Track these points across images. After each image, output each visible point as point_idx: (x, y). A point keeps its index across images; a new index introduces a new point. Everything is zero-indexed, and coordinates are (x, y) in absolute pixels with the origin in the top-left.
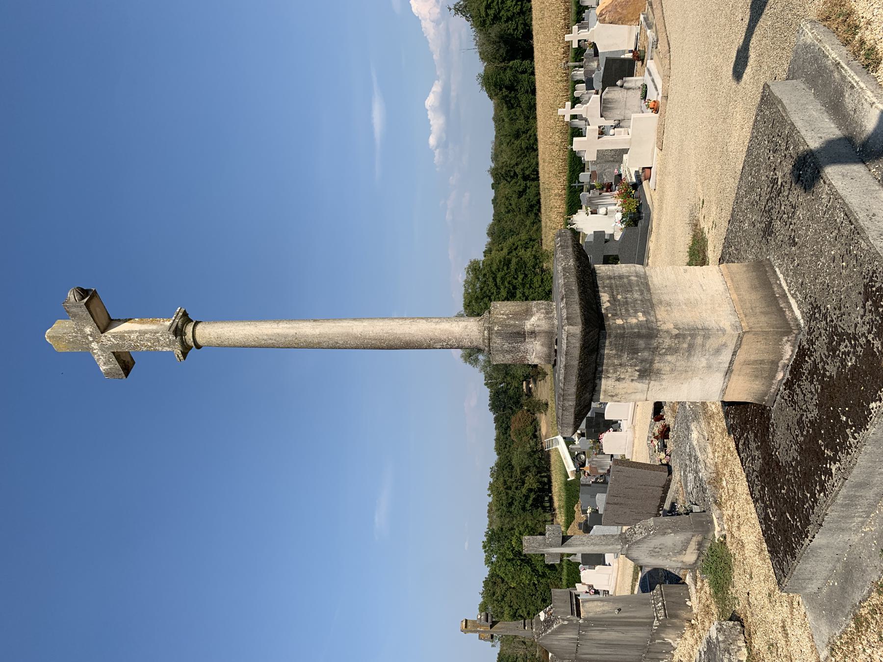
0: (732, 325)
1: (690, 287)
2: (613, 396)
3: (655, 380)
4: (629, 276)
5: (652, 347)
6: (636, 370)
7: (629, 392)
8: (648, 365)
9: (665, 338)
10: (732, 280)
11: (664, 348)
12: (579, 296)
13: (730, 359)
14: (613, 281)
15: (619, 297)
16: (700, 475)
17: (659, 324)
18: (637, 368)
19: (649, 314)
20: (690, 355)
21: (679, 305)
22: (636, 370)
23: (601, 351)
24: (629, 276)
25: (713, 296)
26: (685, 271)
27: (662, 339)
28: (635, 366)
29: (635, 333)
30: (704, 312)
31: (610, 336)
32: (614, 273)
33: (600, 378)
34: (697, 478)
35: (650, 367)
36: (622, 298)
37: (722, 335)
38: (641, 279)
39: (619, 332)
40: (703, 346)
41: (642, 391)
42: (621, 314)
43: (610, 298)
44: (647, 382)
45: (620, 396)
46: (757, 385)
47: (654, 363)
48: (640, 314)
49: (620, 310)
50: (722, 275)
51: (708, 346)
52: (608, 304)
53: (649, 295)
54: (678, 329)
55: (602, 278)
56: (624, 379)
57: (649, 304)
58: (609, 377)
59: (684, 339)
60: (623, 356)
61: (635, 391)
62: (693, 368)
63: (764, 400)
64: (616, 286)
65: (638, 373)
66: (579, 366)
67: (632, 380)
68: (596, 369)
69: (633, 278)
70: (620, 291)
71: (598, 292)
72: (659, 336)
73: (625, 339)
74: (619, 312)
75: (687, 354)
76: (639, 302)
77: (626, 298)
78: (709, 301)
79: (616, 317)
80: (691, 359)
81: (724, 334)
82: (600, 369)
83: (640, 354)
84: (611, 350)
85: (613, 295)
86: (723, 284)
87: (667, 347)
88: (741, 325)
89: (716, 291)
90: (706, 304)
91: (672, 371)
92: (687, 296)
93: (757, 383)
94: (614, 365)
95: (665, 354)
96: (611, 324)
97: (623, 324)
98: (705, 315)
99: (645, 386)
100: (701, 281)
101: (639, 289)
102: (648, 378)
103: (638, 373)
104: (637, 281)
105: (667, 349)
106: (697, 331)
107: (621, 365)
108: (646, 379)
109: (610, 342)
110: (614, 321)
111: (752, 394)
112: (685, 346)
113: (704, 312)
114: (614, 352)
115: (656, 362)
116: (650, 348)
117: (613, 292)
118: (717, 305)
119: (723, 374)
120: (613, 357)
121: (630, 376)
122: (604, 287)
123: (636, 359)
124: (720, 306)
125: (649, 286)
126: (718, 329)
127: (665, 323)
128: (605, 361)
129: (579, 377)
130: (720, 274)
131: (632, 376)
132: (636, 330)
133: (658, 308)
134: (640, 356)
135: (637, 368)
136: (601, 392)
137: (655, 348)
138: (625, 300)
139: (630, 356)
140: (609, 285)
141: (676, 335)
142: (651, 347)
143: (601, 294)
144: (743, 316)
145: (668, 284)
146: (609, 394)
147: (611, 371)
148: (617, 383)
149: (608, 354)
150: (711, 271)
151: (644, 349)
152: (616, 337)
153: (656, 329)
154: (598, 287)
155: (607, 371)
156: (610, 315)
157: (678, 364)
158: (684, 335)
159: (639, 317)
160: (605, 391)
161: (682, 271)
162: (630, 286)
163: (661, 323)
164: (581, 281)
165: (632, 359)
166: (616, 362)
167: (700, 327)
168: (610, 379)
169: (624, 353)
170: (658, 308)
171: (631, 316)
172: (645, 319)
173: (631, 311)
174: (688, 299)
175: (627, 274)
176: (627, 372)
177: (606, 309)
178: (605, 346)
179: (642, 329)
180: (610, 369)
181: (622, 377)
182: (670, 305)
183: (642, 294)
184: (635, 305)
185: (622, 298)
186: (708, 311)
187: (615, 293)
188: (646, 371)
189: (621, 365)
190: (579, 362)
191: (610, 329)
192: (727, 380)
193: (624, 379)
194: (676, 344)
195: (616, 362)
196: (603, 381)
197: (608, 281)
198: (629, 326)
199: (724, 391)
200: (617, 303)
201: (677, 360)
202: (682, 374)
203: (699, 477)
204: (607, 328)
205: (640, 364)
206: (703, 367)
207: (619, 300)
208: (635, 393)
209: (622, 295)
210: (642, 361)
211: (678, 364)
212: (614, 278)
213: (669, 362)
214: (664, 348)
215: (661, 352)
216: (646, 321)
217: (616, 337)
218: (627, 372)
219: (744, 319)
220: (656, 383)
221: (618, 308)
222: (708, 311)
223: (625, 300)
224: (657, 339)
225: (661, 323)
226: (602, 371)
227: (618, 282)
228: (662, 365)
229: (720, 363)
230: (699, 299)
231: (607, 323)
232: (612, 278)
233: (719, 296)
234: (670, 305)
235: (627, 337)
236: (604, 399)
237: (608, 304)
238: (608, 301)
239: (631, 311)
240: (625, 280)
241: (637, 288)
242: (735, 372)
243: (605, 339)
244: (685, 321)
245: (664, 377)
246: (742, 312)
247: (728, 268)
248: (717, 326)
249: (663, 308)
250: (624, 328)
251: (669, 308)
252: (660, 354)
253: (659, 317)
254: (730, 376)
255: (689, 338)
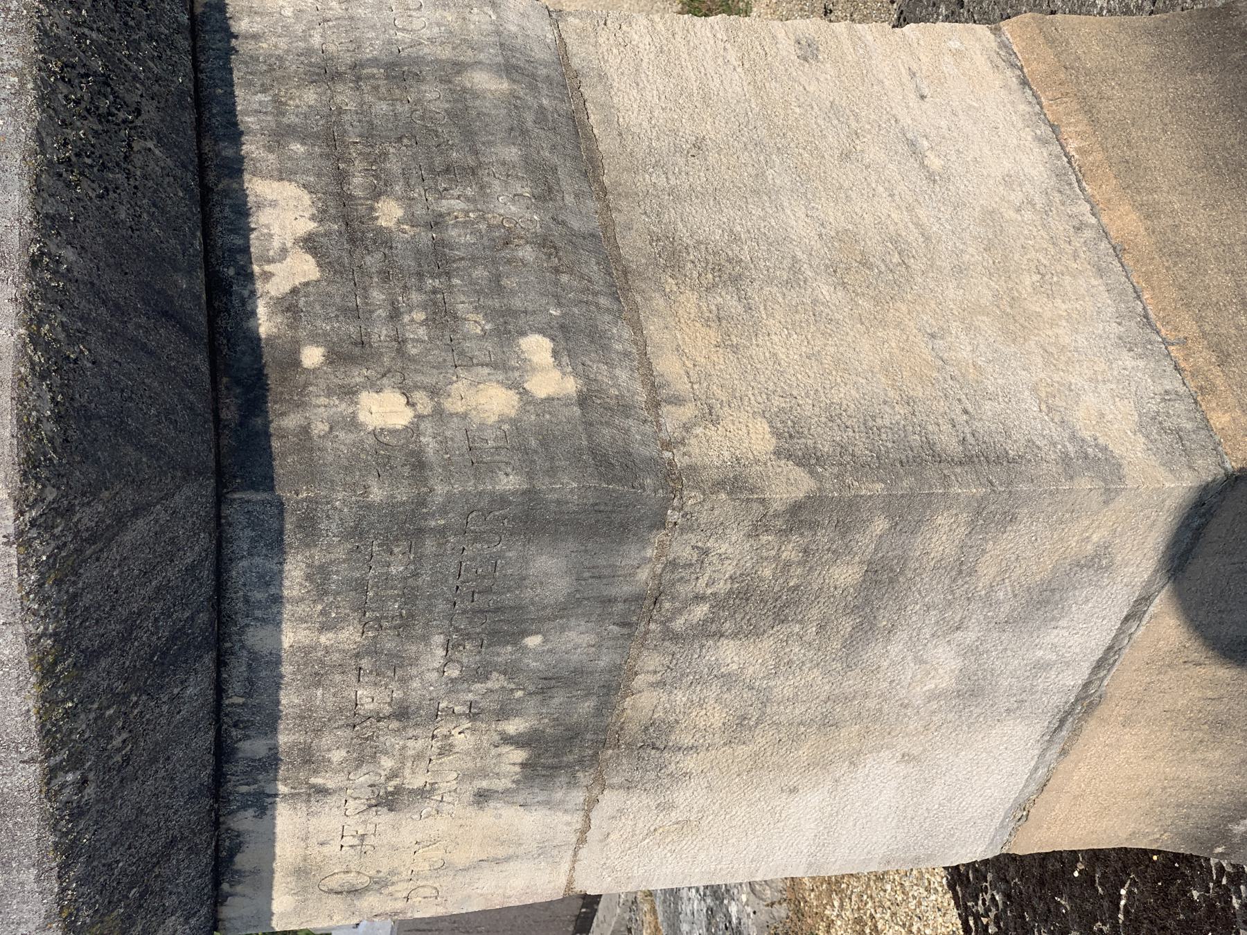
0: (1150, 424)
1: (845, 156)
2: (354, 892)
3: (628, 786)
4: (459, 67)
5: (627, 589)
6: (507, 740)
7: (460, 857)
8: (587, 706)
9: (717, 529)
10: (1089, 110)
11: (699, 598)
12: (38, 190)
13: (1108, 641)
14: (345, 97)
15: (389, 213)
16: (733, 909)
17: (672, 419)
18: (513, 727)
19: (598, 339)
20: (866, 630)
21: (794, 279)
22: (507, 740)
23: (256, 637)
24: (459, 67)
25: (990, 215)
26: (808, 51)
27: (693, 538)
28: (503, 713)
29: (502, 500)
30: (955, 326)
31: (309, 525)
32: (358, 45)
33: (263, 804)
34: (719, 918)
35: (598, 712)
36: (412, 220)
37: (1096, 497)
38: (533, 88)
39: (377, 494)
40: (962, 569)
41: (544, 851)
42: (401, 341)
43: (321, 216)
44: (578, 796)
45: (401, 889)
46: (1210, 766)
47: (630, 692)
48: (537, 347)
49: (395, 315)
50: (1024, 83)
51: (987, 570)
52: (304, 268)
53: (592, 205)
54: (808, 460)
55: (274, 71)
56: (423, 793)
57: (593, 268)
58: (322, 791)
59: (844, 529)
60: (414, 662)
61: (501, 852)
62: (871, 704)
63: (1225, 837)
64: (370, 135)
65: (519, 755)
66: (50, 795)
67: (482, 797)
68: (222, 752)
69: (485, 82)
70: (394, 166)
71: (235, 168)
72: (673, 516)
73: (430, 546)
74: (381, 333)
75: (847, 625)
76: (527, 253)
77: (436, 222)
78: (973, 254)
79: (358, 375)
80: (873, 653)
81: (1109, 495)
82: (253, 747)
83: (533, 641)
84: (324, 628)
85: (345, 199)
86: (1043, 142)
87: (722, 587)
88: (1208, 427)
89: (1008, 181)
90: (960, 270)
91: (739, 728)
92: (835, 217)
93: (1216, 755)
94: (354, 718)
95: (707, 632)
96: (320, 428)
97: (413, 430)
98: (965, 353)
99: (563, 823)
100: (906, 121)
101: (526, 159)
102: (584, 778)
103: (519, 755)
104: (513, 103)
105: (719, 603)
106: (931, 473)
107: (402, 713)
108: (573, 783)
109: (319, 577)
110: (343, 407)
111: (1170, 812)
112: (846, 575)
113: (955, 326)
114: (349, 636)
115: (640, 681)
116: (611, 601)
117: (341, 177)
118: (1029, 280)
119: (1040, 727)
120: (342, 668)
121: (465, 777)
122: (279, 136)
123: (510, 671)
124: (1047, 285)
125: (591, 138)
126: (1065, 459)
127: (710, 416)
128: (289, 699)
129: (64, 867)
130: (1012, 77)
131: (483, 773)
132: (509, 482)
133: (659, 302)
134: (538, 655)
135: (513, 727)
136: (278, 877)
137: (638, 598)
138: (426, 237)
139: (468, 655)
140: (317, 125)
141: (796, 508)
142: (613, 591)
143: (258, 187)
144: (1203, 357)
145: (707, 129)
146: (334, 883)
147: (337, 756)
148: (384, 818)
149: (307, 651)
150: (956, 54)
151: (564, 610)
152: (356, 532)
153: (652, 464)
154: (234, 133)
155: (309, 758)
156: (312, 356)
157: (783, 687)
158: (853, 505)
159: (526, 367)
160: (301, 872)
161: (787, 47)
162: (468, 135)
163: (687, 412)
164: (69, 73)
165: (480, 673)
166: (369, 697)
167: (948, 442)
168: (332, 800)
169: (425, 638)
170: (659, 302)
171: (469, 363)
172: (571, 386)
173: (475, 324)
174: (846, 238)
175: (446, 53)
176: (446, 750)
177: (289, 305)
178: (277, 600)
179: (552, 472)
180: (326, 740)
181: (416, 781)
182: (735, 280)
183: (546, 194)
184: (496, 279)
185: (412, 220)
186: (983, 322)
187: (358, 183)
188: (571, 736)
189: (402, 713)
190: (51, 774)
191: (312, 474)
192: (1056, 749)
193: (423, 793)
194: (788, 565)
195: (369, 697)
196: (286, 819)
197: (310, 96)
198: (460, 441)
199: (1022, 813)
200: (372, 261)
201: (782, 665)
202: (796, 739)
203: (728, 916)
204: (285, 464)
205: (532, 702)
206: (933, 696)
207: (384, 240)
208: (498, 861)
209: (408, 201)
210: (547, 684)
211: (783, 687)
212: (356, 72)
213: (729, 680)
214: (699, 598)
215: (679, 624)
216: (583, 400)
217: (356, 532)
218: (446, 750)
219: (1216, 373)
220: (637, 801)
221: (377, 296)
222: (983, 322)
223: (426, 237)
224: (659, 536)
225: (687, 412)
226: (271, 762)
227: (384, 107)
228: (680, 697)
229: (1042, 667)
230: (913, 236)
231: (291, 422)
232: (336, 77)
233: (1028, 215)
234: (735, 280)
235: (442, 532)
236: (297, 911)
237: (304, 268)
238: (310, 243)
239: (475, 324)
240: (432, 94)
241: (512, 153)
242: (1113, 710)
243: (277, 546)
244: (844, 394)
245: (690, 763)
246: (1190, 327)
247: (1051, 42)
248: (1054, 431)
249: (689, 301)
250: (419, 464)
251: (727, 300)
252: (675, 637)
253: (668, 366)
254: (1076, 732)
255: (880, 525)
